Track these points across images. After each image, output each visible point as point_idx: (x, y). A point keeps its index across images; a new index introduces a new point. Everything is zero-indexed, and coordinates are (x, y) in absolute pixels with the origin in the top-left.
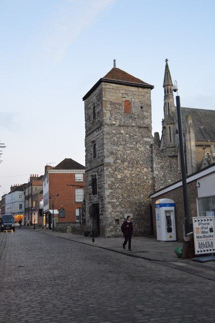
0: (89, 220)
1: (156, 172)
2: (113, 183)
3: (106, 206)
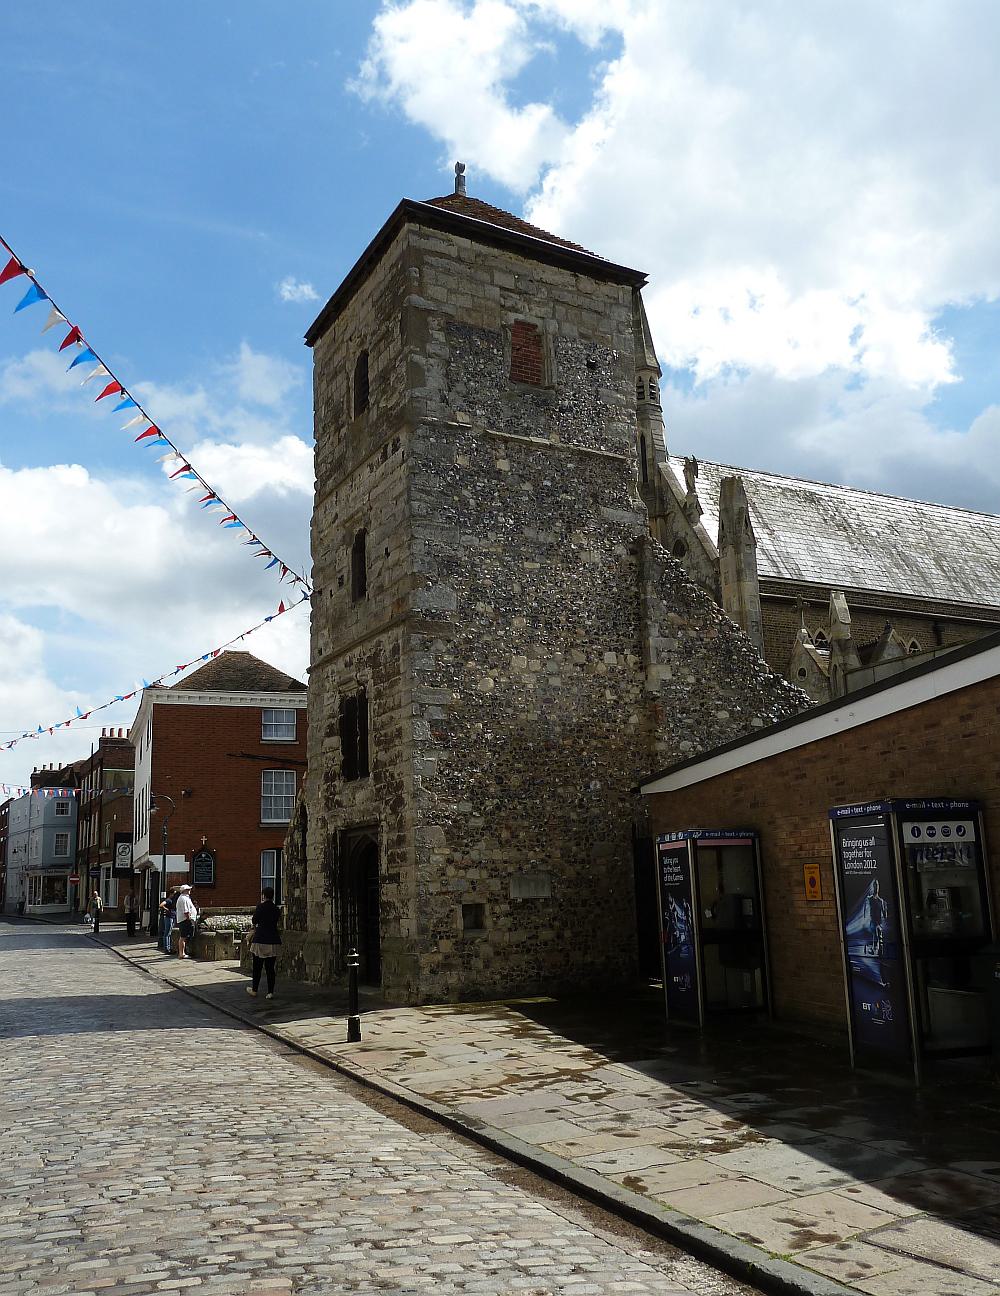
1: (660, 673)
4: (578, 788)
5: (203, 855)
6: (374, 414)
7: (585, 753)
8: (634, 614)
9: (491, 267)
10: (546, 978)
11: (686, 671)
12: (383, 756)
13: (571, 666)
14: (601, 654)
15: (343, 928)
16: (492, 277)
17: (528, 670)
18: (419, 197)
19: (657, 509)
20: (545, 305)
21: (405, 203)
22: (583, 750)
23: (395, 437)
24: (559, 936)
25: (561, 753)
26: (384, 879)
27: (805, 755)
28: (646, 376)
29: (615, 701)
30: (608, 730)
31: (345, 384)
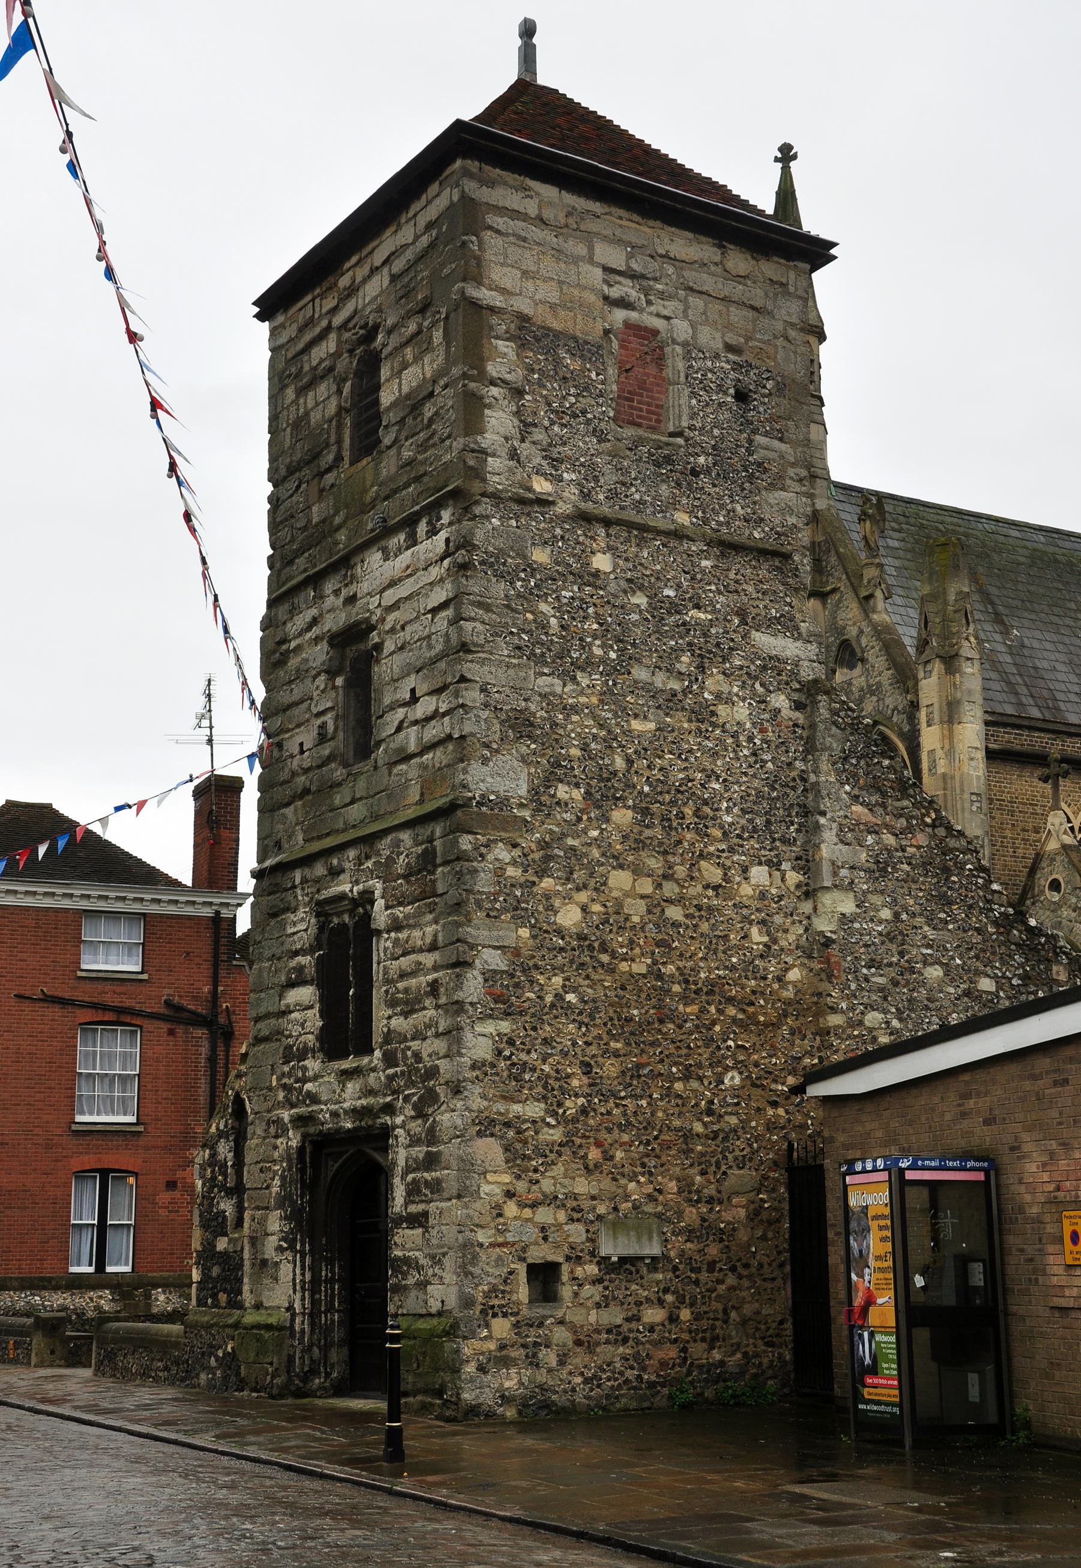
2: (522, 968)
4: (706, 1083)
7: (717, 1028)
8: (799, 805)
14: (745, 870)
16: (591, 249)
22: (714, 1023)
24: (673, 1319)
26: (399, 1221)
29: (765, 945)
30: (754, 992)
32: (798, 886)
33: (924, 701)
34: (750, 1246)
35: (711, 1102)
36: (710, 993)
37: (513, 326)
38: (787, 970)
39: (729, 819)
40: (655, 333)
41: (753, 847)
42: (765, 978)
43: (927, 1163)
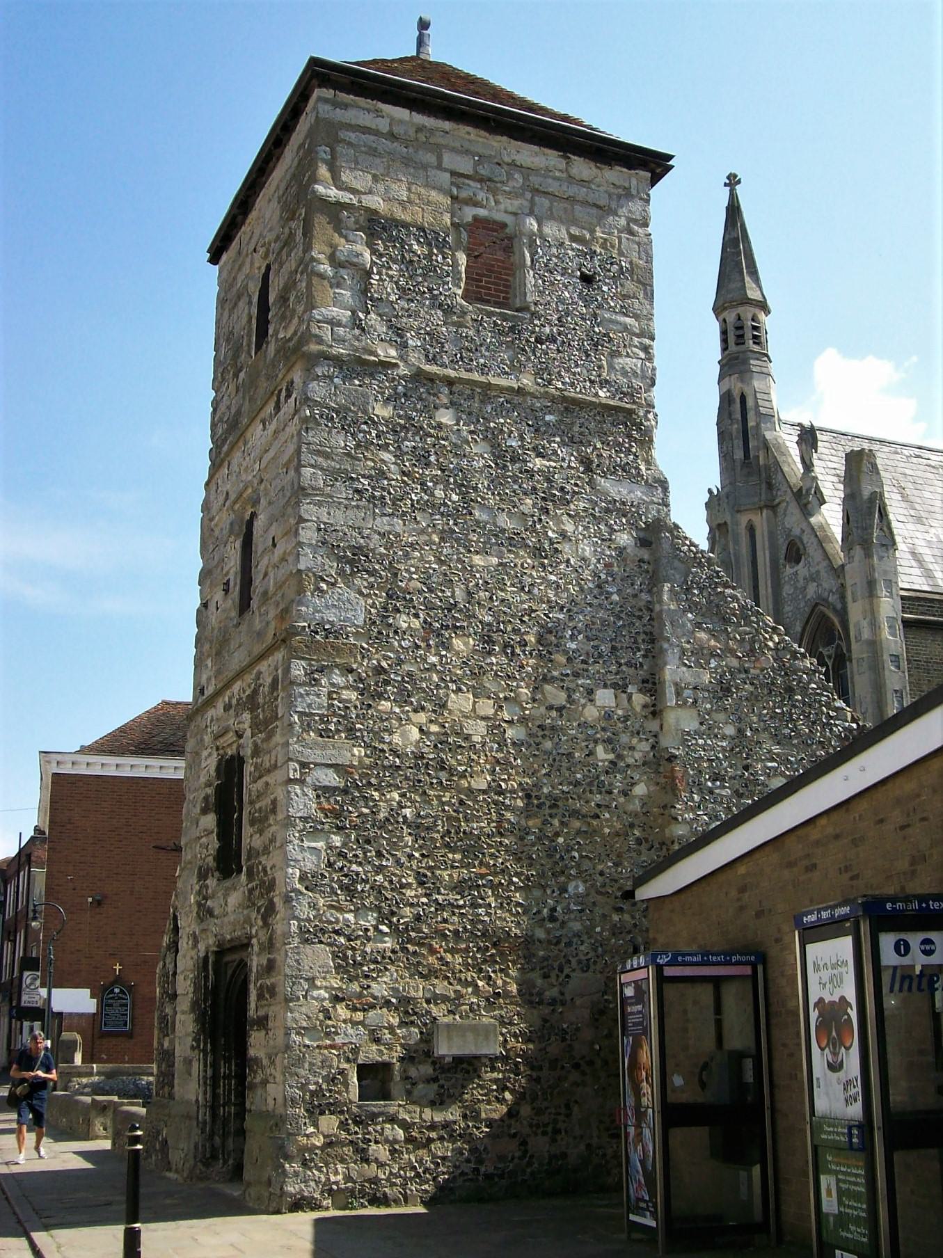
0: (188, 1062)
3: (287, 964)
4: (549, 892)
5: (117, 990)
6: (272, 349)
7: (561, 840)
8: (645, 633)
9: (438, 145)
10: (488, 1177)
11: (721, 717)
12: (257, 842)
13: (543, 709)
14: (590, 692)
15: (215, 1096)
16: (440, 158)
17: (474, 714)
18: (345, 51)
19: (763, 496)
20: (517, 196)
21: (314, 62)
22: (557, 834)
23: (288, 378)
25: (522, 839)
27: (814, 833)
28: (747, 312)
29: (611, 762)
30: (598, 806)
31: (246, 311)
32: (645, 706)
33: (849, 582)
34: (593, 1044)
35: (554, 910)
36: (554, 806)
37: (362, 219)
38: (633, 784)
39: (573, 646)
40: (504, 225)
41: (598, 672)
42: (610, 793)
43: (688, 958)
